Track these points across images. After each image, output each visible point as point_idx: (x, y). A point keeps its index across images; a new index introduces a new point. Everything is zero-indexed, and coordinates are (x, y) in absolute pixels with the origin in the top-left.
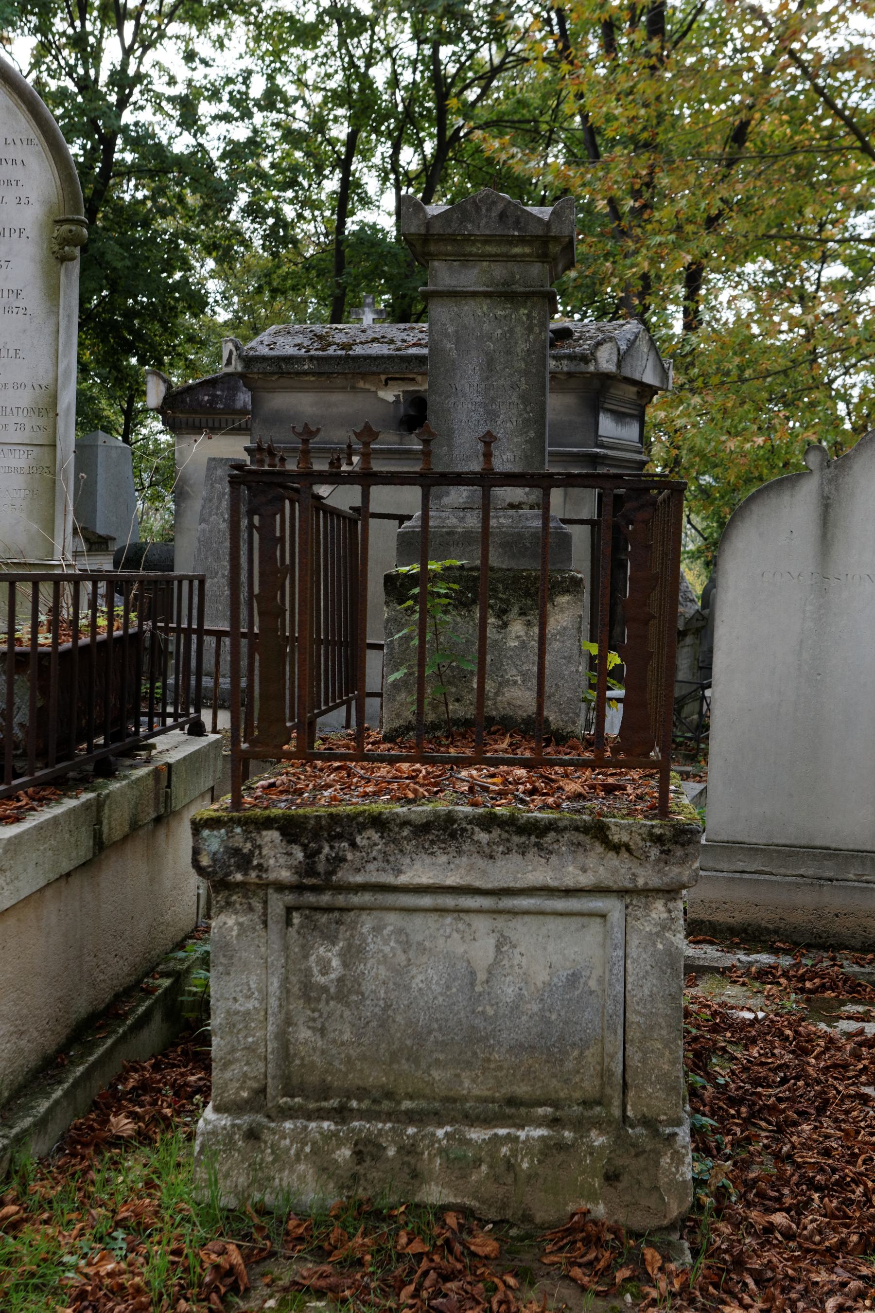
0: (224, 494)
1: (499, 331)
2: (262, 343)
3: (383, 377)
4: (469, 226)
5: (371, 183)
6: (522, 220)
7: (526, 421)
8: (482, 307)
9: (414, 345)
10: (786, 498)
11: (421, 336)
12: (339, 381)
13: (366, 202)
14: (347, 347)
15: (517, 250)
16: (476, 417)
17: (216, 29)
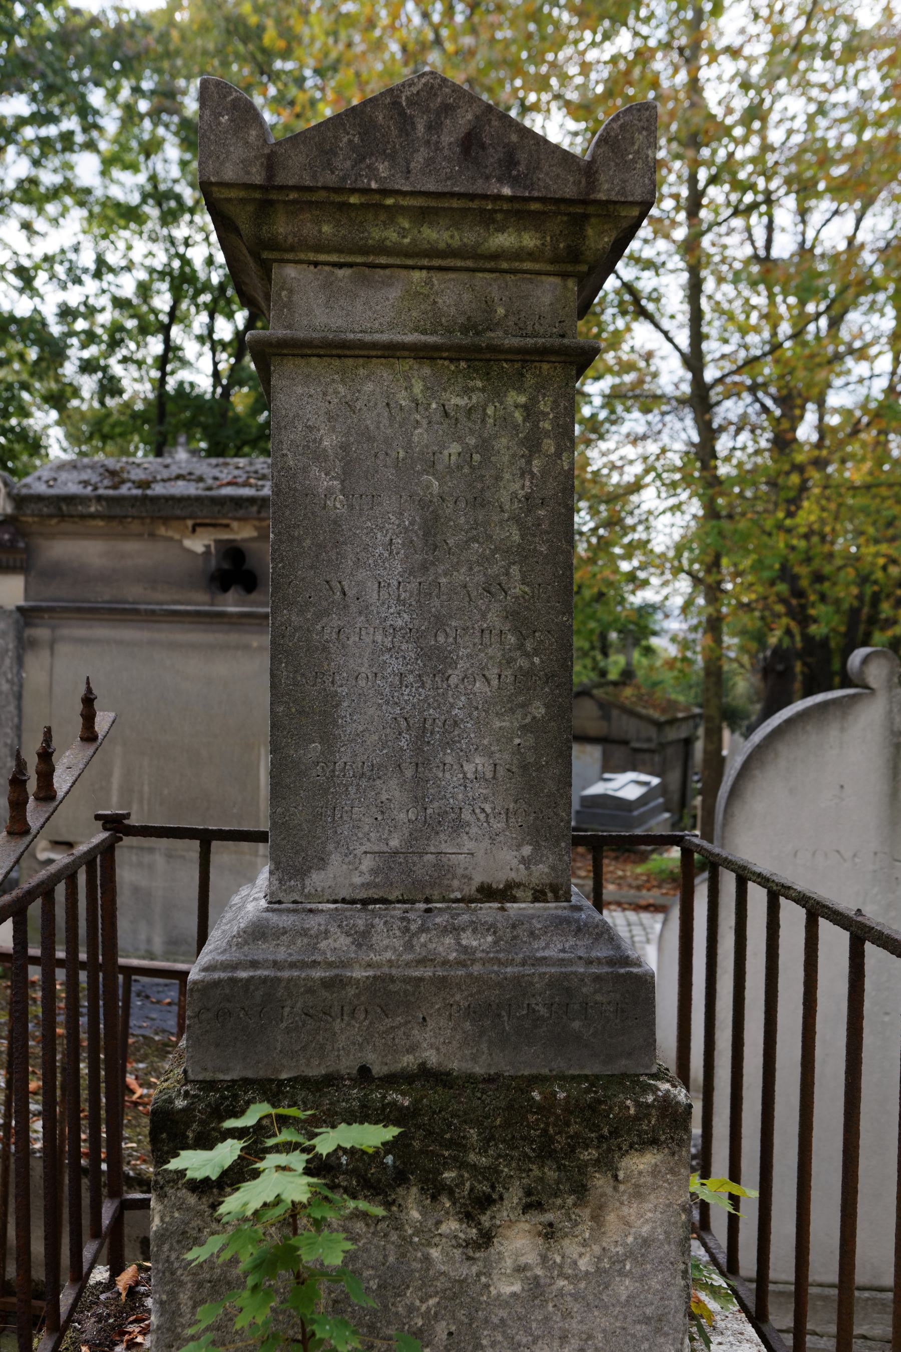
0: (7, 651)
1: (455, 448)
2: (39, 478)
3: (190, 523)
4: (383, 168)
5: (191, 349)
6: (522, 156)
7: (525, 677)
8: (418, 379)
9: (229, 484)
10: (833, 732)
11: (236, 472)
12: (135, 527)
13: (185, 363)
14: (145, 484)
15: (503, 240)
16: (396, 665)
17: (51, 209)
